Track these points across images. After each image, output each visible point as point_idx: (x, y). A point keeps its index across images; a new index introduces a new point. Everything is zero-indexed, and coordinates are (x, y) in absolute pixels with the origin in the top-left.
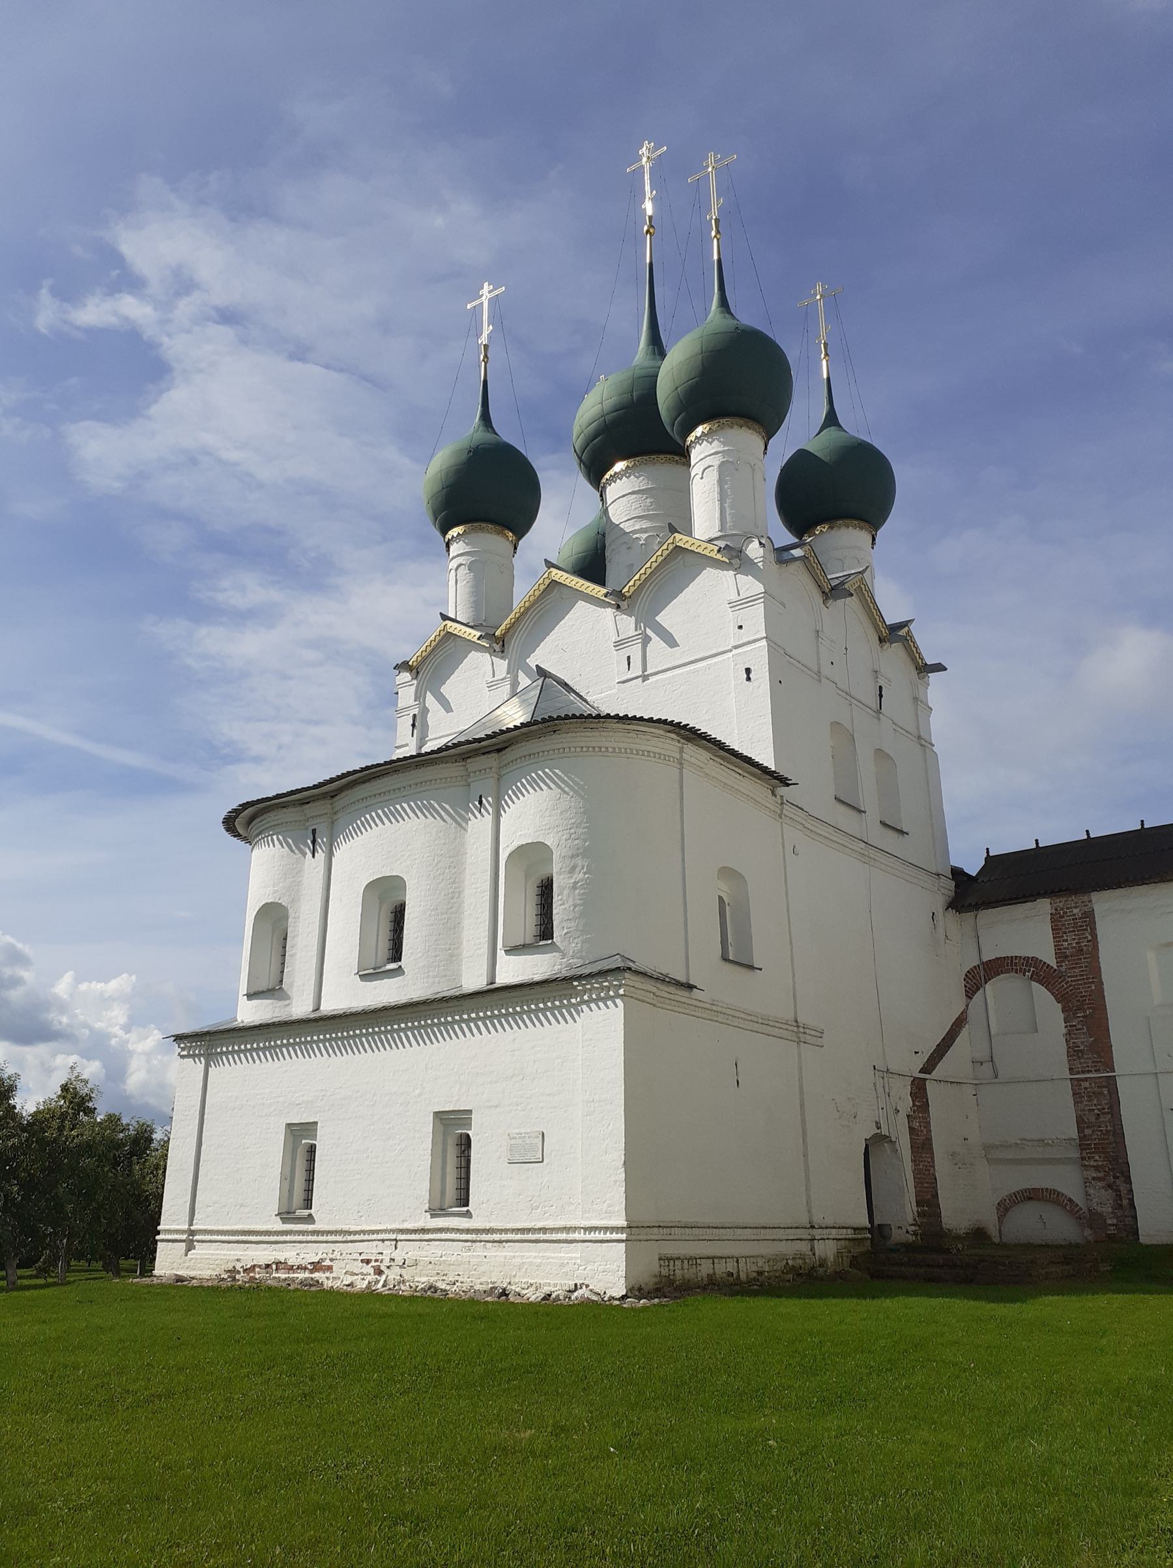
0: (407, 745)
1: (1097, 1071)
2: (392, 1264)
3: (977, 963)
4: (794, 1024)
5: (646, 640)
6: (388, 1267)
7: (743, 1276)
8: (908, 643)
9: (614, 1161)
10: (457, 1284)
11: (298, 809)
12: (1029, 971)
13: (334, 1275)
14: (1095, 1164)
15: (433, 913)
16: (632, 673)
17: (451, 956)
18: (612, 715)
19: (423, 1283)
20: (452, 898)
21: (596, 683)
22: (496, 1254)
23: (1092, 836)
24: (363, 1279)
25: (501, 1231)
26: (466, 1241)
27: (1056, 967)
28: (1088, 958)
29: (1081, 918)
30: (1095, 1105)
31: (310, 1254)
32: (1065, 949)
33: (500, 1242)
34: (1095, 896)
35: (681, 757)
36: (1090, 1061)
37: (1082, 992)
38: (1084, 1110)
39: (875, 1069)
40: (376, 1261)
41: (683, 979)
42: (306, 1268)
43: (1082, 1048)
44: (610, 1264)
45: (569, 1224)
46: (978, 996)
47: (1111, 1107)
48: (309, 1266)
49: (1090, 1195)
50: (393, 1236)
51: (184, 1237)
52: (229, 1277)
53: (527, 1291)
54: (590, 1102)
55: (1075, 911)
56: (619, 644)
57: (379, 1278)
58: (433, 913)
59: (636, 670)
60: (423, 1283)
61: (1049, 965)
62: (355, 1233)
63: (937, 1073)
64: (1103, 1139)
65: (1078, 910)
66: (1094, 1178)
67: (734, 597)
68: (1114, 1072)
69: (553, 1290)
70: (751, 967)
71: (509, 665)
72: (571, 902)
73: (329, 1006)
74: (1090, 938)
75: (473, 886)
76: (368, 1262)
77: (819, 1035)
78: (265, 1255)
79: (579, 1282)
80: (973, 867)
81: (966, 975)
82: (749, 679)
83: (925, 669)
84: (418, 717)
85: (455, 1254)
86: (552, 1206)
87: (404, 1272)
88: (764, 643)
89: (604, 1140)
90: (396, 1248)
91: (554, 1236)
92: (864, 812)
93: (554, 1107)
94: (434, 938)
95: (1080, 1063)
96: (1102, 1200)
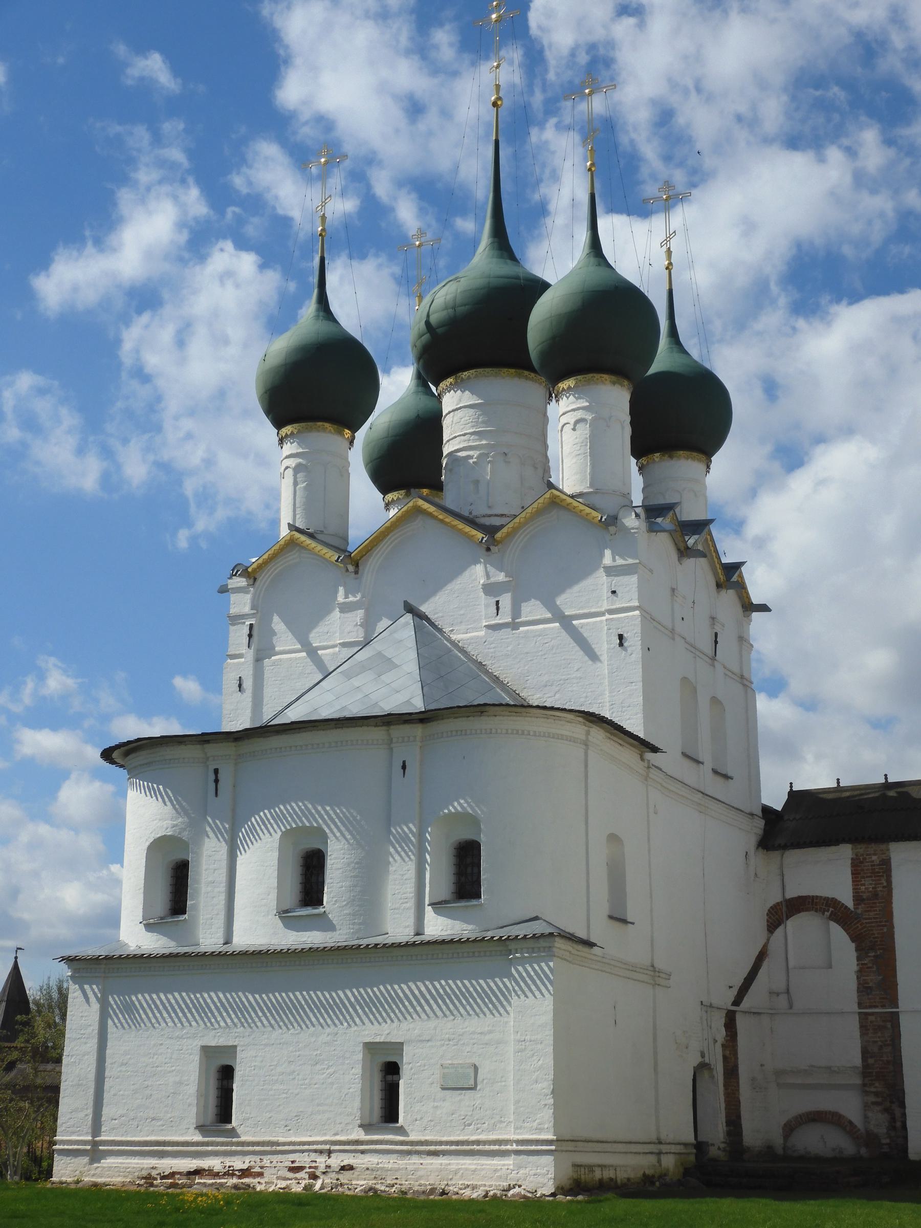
1: (883, 1006)
2: (328, 1170)
3: (779, 899)
4: (651, 969)
6: (324, 1173)
7: (619, 1181)
8: (741, 588)
9: (544, 1089)
10: (396, 1186)
11: (198, 746)
13: (266, 1179)
16: (500, 619)
19: (361, 1186)
21: (461, 622)
23: (890, 780)
24: (298, 1183)
28: (882, 903)
30: (879, 1037)
31: (239, 1163)
32: (862, 892)
35: (587, 739)
39: (702, 1004)
40: (310, 1167)
41: (582, 934)
42: (233, 1175)
44: (540, 1169)
45: (501, 1137)
46: (779, 931)
48: (237, 1173)
50: (327, 1147)
52: (146, 1183)
53: (464, 1191)
54: (522, 1041)
55: (874, 858)
57: (314, 1182)
60: (361, 1186)
62: (284, 1144)
63: (746, 1004)
68: (898, 1008)
69: (488, 1189)
70: (624, 921)
77: (667, 977)
78: (184, 1163)
80: (778, 804)
81: (769, 910)
82: (621, 644)
83: (749, 607)
85: (391, 1161)
86: (484, 1123)
87: (340, 1177)
89: (534, 1072)
92: (702, 763)
96: (878, 1122)
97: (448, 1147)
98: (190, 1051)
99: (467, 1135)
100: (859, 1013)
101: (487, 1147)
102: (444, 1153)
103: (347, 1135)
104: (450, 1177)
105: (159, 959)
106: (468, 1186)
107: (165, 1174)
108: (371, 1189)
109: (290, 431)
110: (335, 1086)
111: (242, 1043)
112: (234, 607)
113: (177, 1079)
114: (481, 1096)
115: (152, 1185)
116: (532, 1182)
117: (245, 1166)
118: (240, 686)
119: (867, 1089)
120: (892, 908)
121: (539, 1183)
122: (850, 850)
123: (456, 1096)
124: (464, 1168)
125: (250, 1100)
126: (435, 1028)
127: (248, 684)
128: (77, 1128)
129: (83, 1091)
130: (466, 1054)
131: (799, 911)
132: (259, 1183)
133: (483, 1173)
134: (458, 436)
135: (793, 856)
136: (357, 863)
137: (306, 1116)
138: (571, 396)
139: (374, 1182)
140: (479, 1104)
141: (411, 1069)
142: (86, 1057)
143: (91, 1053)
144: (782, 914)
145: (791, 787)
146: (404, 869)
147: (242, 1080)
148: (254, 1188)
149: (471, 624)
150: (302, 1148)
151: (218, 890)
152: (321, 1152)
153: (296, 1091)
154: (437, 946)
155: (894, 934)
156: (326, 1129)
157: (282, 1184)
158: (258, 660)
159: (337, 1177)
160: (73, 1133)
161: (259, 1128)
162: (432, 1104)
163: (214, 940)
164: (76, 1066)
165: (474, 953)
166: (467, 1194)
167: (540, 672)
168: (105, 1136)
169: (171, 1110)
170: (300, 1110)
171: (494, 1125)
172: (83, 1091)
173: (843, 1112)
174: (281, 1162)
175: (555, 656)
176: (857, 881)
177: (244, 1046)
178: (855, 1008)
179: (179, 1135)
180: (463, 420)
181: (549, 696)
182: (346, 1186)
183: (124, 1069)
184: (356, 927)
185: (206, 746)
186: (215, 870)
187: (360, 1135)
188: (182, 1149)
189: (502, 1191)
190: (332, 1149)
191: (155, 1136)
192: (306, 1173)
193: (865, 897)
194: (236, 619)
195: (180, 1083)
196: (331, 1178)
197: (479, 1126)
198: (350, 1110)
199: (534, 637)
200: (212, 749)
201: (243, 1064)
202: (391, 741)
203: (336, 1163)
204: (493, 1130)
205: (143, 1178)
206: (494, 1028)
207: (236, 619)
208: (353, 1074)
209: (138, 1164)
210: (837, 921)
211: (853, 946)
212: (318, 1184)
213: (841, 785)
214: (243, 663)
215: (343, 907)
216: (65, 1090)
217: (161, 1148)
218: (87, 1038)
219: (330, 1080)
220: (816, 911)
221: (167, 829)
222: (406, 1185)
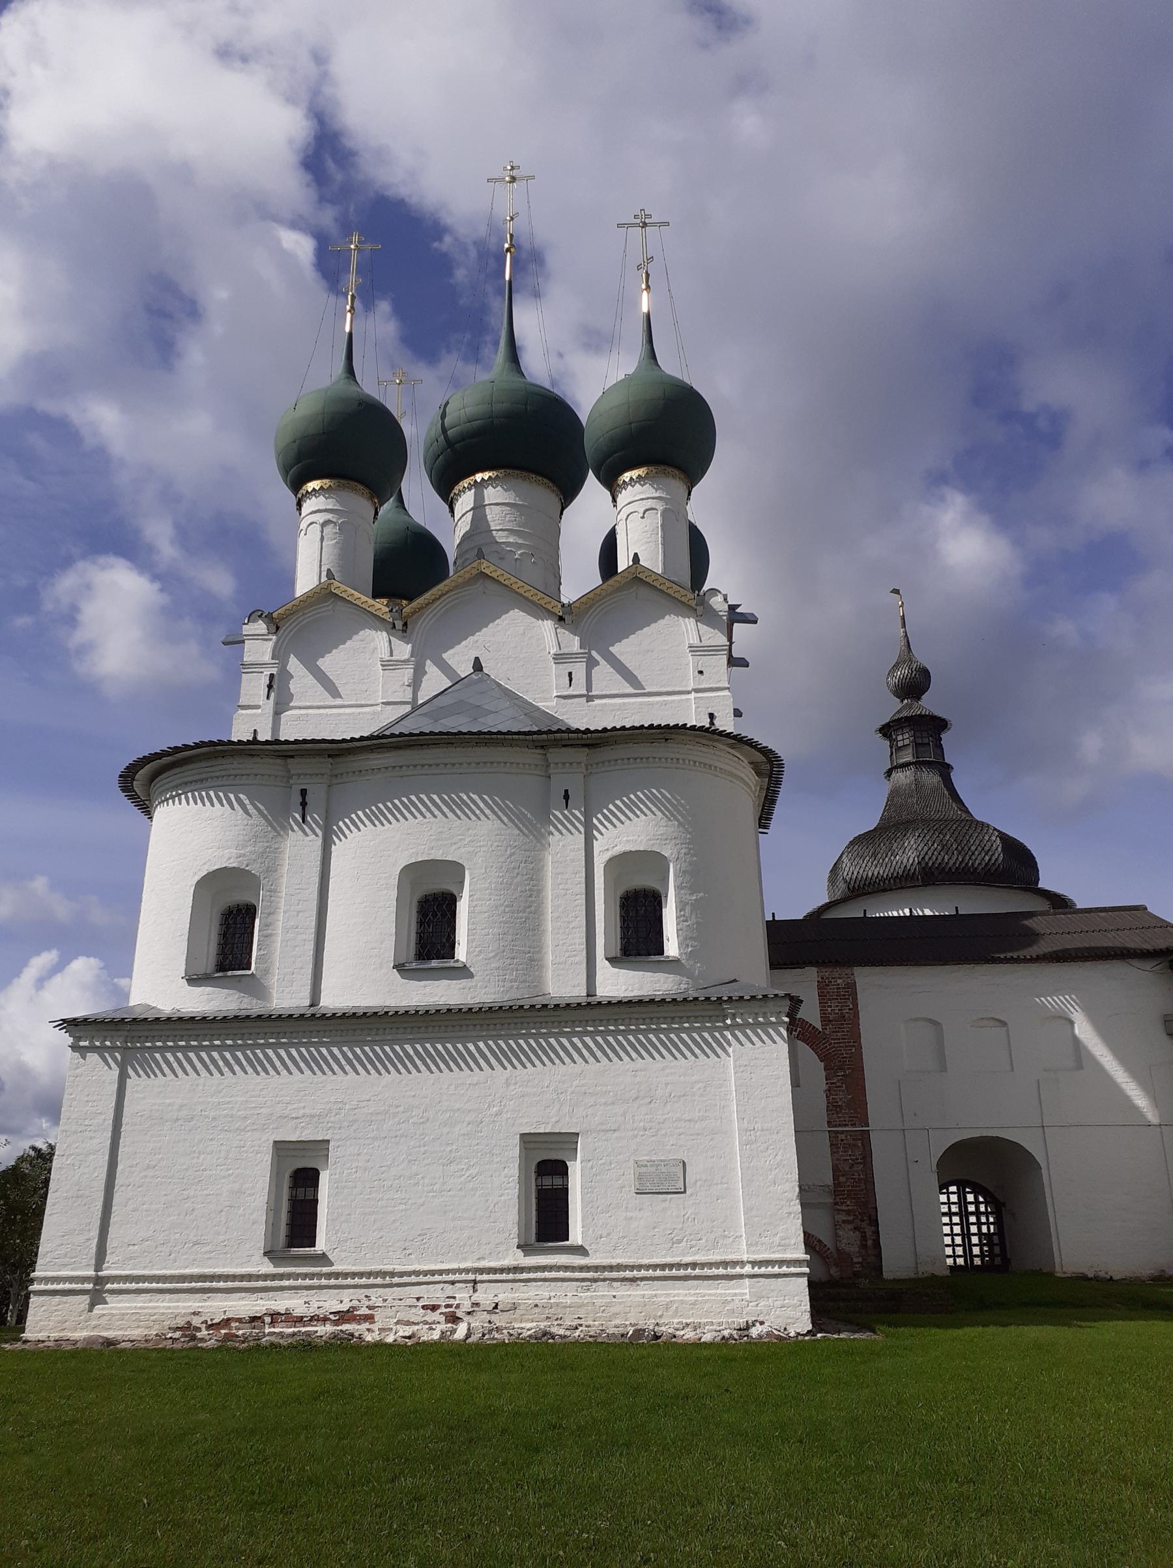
0: (257, 707)
1: (854, 1125)
5: (591, 664)
6: (469, 1313)
10: (581, 1328)
11: (279, 761)
12: (796, 1031)
14: (846, 1208)
15: (507, 910)
16: (573, 691)
17: (531, 960)
18: (609, 728)
19: (528, 1330)
20: (530, 896)
22: (628, 1293)
24: (431, 1329)
25: (632, 1268)
26: (583, 1280)
27: (821, 1030)
29: (844, 988)
31: (332, 1302)
32: (829, 1013)
33: (633, 1280)
34: (857, 970)
38: (839, 1160)
40: (447, 1306)
42: (325, 1320)
43: (840, 1104)
47: (864, 1158)
48: (332, 1317)
50: (471, 1277)
51: (90, 1286)
52: (184, 1336)
53: (682, 1333)
56: (559, 658)
57: (455, 1327)
58: (507, 910)
59: (579, 687)
60: (528, 1330)
61: (814, 1027)
62: (402, 1274)
64: (856, 1186)
65: (841, 981)
66: (844, 1222)
67: (696, 642)
68: (868, 1126)
71: (413, 647)
72: (694, 920)
73: (334, 999)
74: (851, 1007)
75: (561, 887)
76: (434, 1308)
79: (751, 1319)
87: (494, 1318)
88: (412, 670)
89: (771, 1170)
90: (475, 1291)
91: (707, 1272)
93: (698, 1134)
94: (510, 938)
95: (839, 1118)
96: (850, 1241)
97: (651, 1273)
98: (256, 1148)
99: (677, 1256)
106: (688, 1325)
107: (214, 1322)
108: (545, 1334)
111: (337, 1137)
115: (193, 1338)
116: (779, 1317)
117: (344, 1307)
119: (838, 1207)
124: (678, 1300)
125: (349, 1215)
126: (624, 1115)
128: (72, 1258)
136: (507, 906)
139: (546, 1323)
140: (691, 1214)
146: (570, 916)
148: (360, 1337)
151: (304, 936)
153: (421, 1201)
154: (623, 1009)
157: (408, 1331)
158: (277, 713)
169: (224, 1229)
172: (85, 1205)
174: (401, 1300)
177: (340, 1140)
183: (151, 1174)
184: (508, 984)
185: (289, 760)
186: (299, 912)
188: (244, 1283)
189: (738, 1330)
192: (440, 1314)
193: (831, 1019)
199: (612, 711)
200: (294, 765)
201: (339, 1164)
206: (707, 1114)
209: (169, 1308)
213: (776, 919)
214: (259, 715)
216: (54, 1205)
218: (95, 1131)
219: (471, 1185)
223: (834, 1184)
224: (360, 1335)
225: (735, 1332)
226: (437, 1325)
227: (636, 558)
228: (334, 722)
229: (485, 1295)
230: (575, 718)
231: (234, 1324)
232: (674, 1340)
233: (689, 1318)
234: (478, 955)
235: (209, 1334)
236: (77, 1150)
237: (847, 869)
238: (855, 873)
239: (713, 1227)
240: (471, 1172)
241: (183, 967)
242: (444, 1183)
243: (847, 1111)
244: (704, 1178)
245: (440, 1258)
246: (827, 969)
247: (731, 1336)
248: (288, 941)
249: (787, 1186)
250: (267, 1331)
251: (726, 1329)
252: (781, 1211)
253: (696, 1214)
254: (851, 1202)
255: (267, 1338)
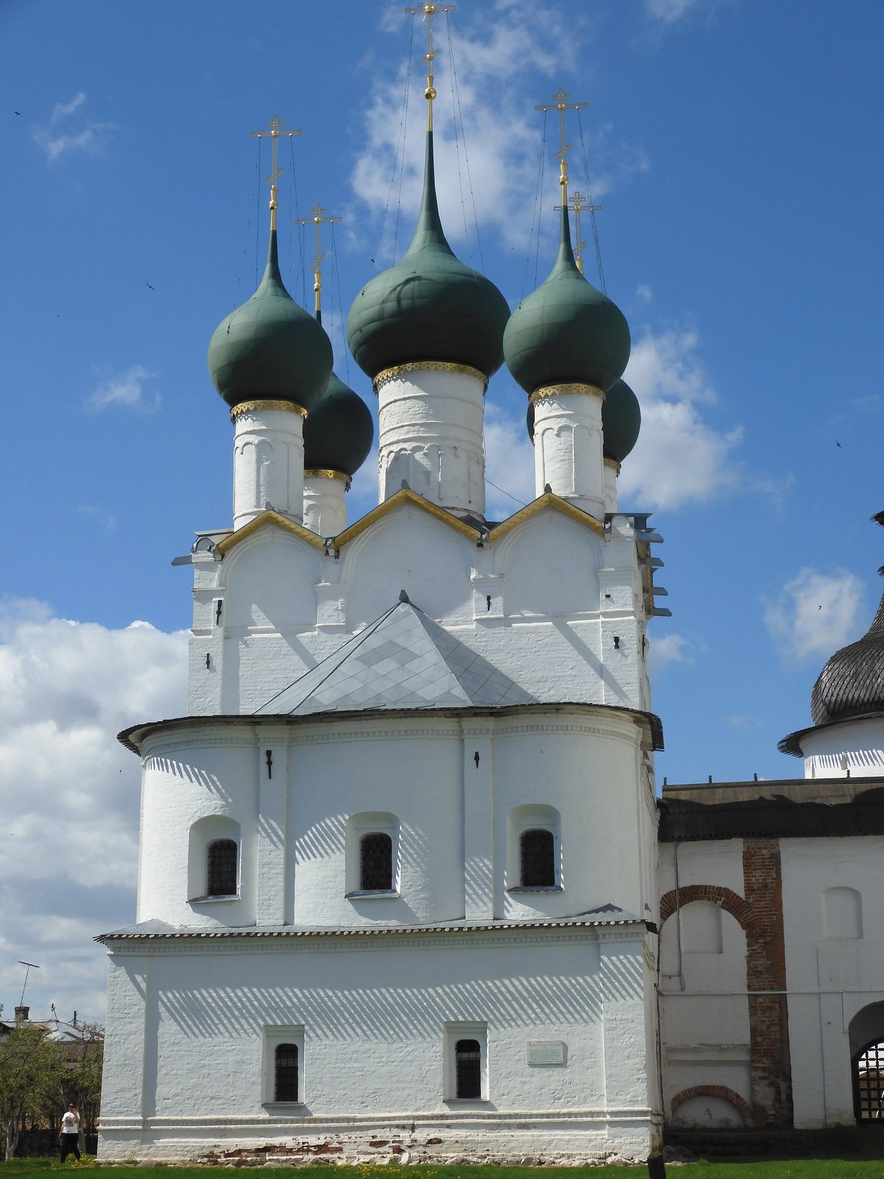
0: (208, 632)
1: (772, 989)
2: (414, 1144)
3: (673, 887)
6: (410, 1147)
9: (636, 1064)
10: (488, 1157)
11: (248, 727)
16: (492, 614)
19: (451, 1158)
24: (383, 1157)
27: (745, 899)
31: (313, 1140)
36: (767, 980)
37: (764, 922)
40: (394, 1142)
42: (308, 1151)
46: (672, 918)
47: (781, 1019)
48: (312, 1149)
49: (755, 1091)
50: (411, 1122)
52: (209, 1161)
53: (559, 1160)
54: (613, 1020)
57: (399, 1155)
60: (451, 1158)
62: (361, 1120)
66: (760, 1078)
81: (662, 898)
82: (617, 647)
84: (224, 605)
86: (575, 1097)
87: (427, 1150)
89: (626, 1048)
95: (758, 982)
96: (765, 1095)
99: (558, 1108)
100: (749, 995)
101: (579, 1119)
102: (535, 1126)
103: (430, 1110)
104: (544, 1147)
105: (252, 938)
106: (563, 1155)
107: (229, 1152)
108: (463, 1161)
109: (246, 408)
110: (414, 1064)
112: (199, 582)
113: (239, 1058)
114: (571, 1072)
115: (216, 1163)
116: (628, 1150)
117: (322, 1142)
118: (208, 663)
120: (781, 898)
121: (636, 1151)
122: (742, 845)
123: (545, 1072)
125: (322, 1078)
127: (217, 661)
128: (125, 1108)
129: (130, 1071)
130: (553, 1032)
131: (692, 899)
132: (339, 1158)
133: (577, 1143)
134: (406, 425)
135: (686, 848)
137: (384, 1093)
138: (546, 403)
139: (464, 1154)
141: (497, 1047)
142: (132, 1036)
143: (139, 1033)
144: (676, 901)
145: (665, 782)
147: (312, 1059)
149: (460, 617)
150: (382, 1123)
151: (275, 871)
152: (404, 1127)
153: (373, 1069)
155: (783, 923)
156: (406, 1105)
157: (367, 1158)
159: (424, 1150)
160: (120, 1113)
161: (332, 1105)
162: (520, 1079)
163: (272, 922)
164: (121, 1046)
165: (558, 937)
166: (564, 1162)
167: (534, 668)
168: (160, 1115)
169: (232, 1088)
170: (378, 1087)
171: (585, 1098)
172: (130, 1071)
173: (730, 1086)
174: (361, 1137)
175: (548, 653)
176: (749, 873)
178: (745, 990)
179: (243, 1114)
180: (411, 410)
181: (543, 691)
182: (435, 1159)
183: (176, 1049)
185: (258, 728)
186: (271, 851)
187: (446, 1110)
190: (415, 1123)
191: (214, 1114)
193: (755, 888)
194: (204, 596)
195: (242, 1062)
196: (418, 1152)
197: (569, 1099)
198: (432, 1086)
199: (527, 633)
200: (263, 731)
202: (462, 731)
203: (422, 1137)
204: (584, 1103)
205: (207, 1156)
207: (204, 596)
208: (434, 1052)
209: (197, 1142)
210: (728, 910)
211: (744, 933)
212: (404, 1158)
215: (418, 891)
217: (223, 1126)
218: (133, 1018)
219: (409, 1058)
220: (709, 900)
221: (216, 808)
222: (498, 1156)
223: (752, 1043)
224: (333, 1161)
225: (596, 1160)
226: (388, 1155)
227: (548, 489)
228: (277, 646)
229: (421, 1135)
230: (493, 641)
231: (244, 1154)
232: (553, 1165)
233: (565, 1151)
234: (409, 888)
235: (227, 1160)
236: (121, 1032)
237: (826, 690)
238: (835, 695)
239: (583, 1088)
240: (408, 1049)
241: (186, 894)
242: (389, 1057)
243: (767, 976)
244: (578, 1054)
245: (388, 1109)
246: (753, 840)
247: (593, 1163)
248: (264, 874)
249: (638, 1060)
250: (267, 1158)
251: (590, 1158)
252: (632, 1078)
253: (572, 1079)
254: (767, 1060)
255: (268, 1163)
